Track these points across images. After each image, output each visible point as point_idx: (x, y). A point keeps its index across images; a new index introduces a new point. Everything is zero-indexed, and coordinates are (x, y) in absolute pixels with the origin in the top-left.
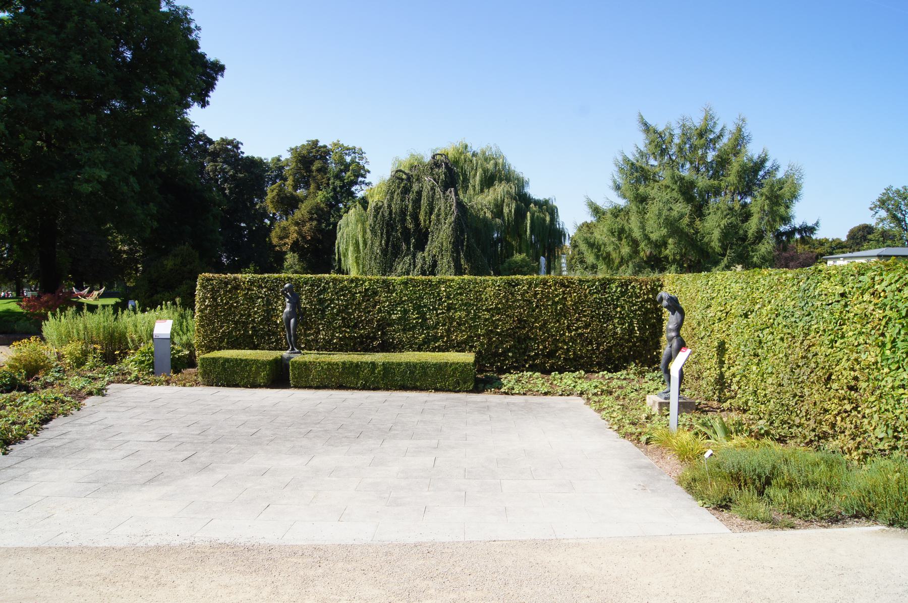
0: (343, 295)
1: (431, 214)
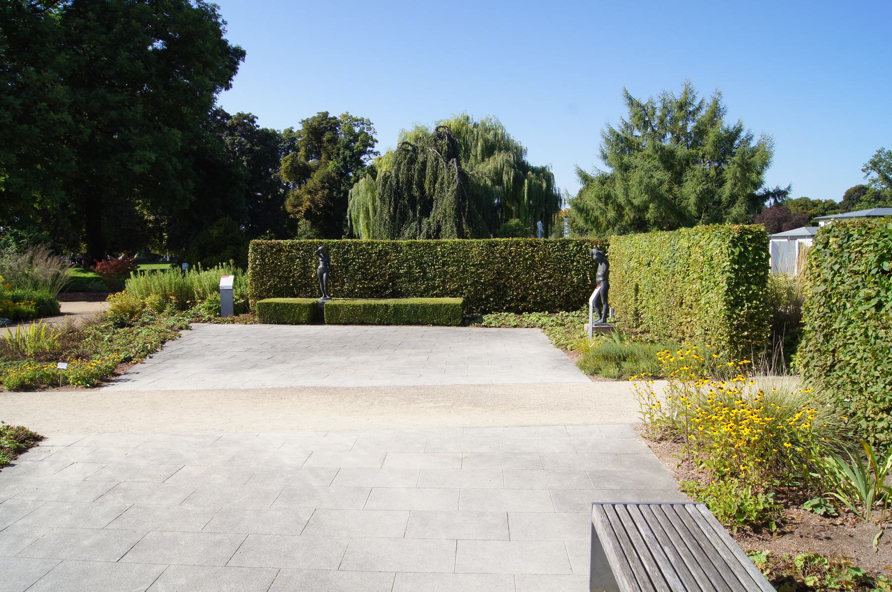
1: (435, 182)
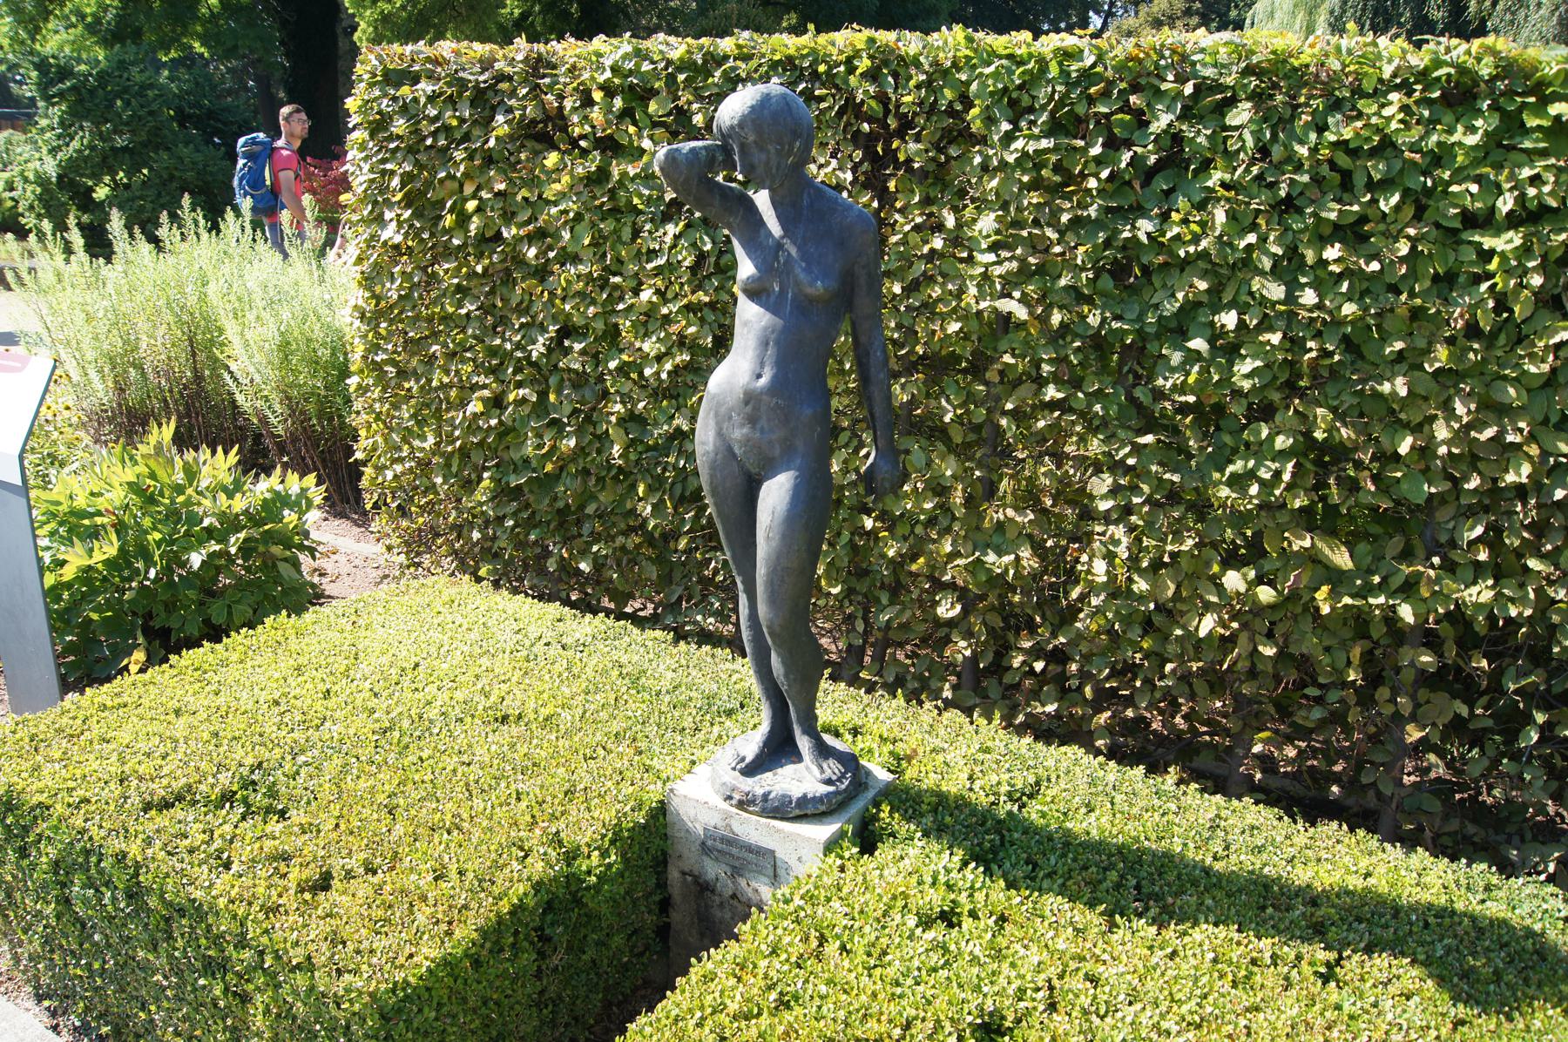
0: (1353, 233)
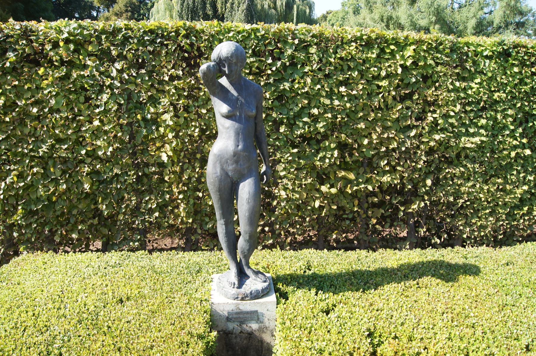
0: (345, 83)
